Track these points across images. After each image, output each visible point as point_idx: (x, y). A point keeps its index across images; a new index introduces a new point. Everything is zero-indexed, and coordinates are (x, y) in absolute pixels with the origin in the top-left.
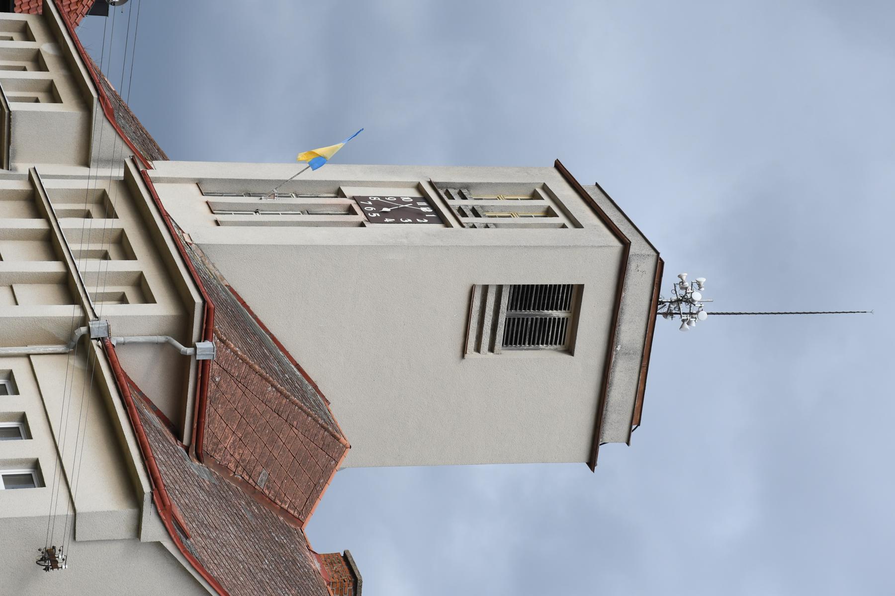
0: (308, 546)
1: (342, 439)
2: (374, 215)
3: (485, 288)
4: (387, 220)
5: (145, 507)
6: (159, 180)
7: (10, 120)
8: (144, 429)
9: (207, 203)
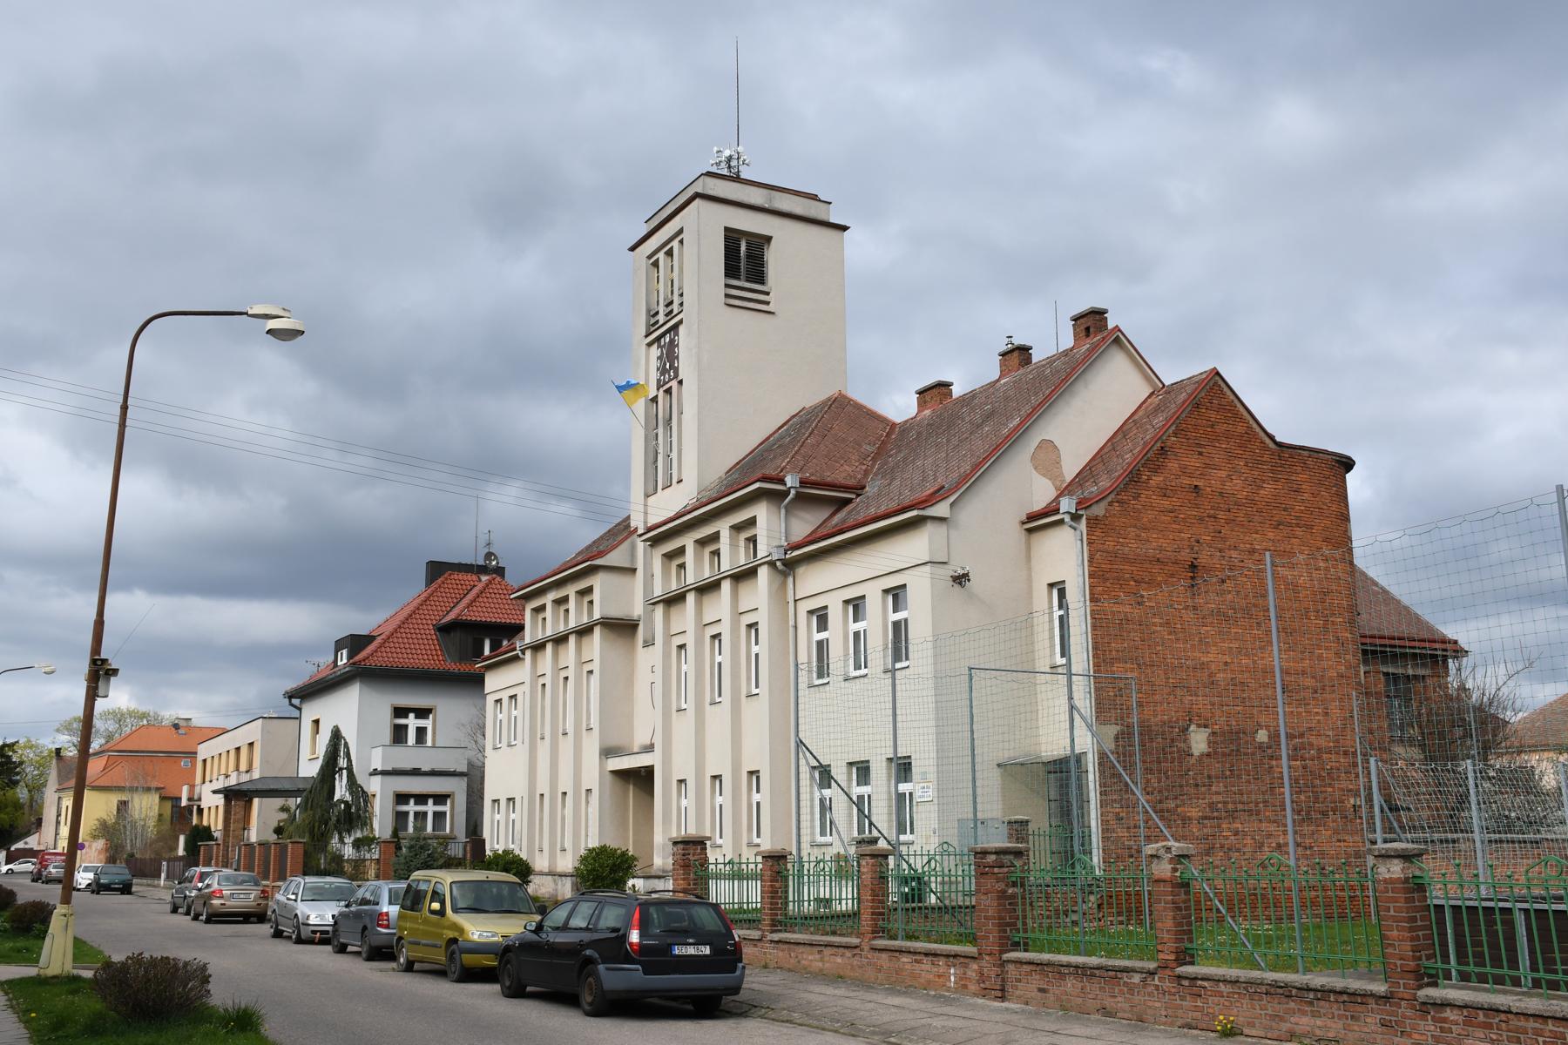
0: (912, 419)
1: (836, 396)
2: (672, 374)
3: (727, 296)
4: (676, 365)
5: (927, 514)
6: (645, 522)
7: (607, 618)
8: (851, 522)
9: (678, 482)
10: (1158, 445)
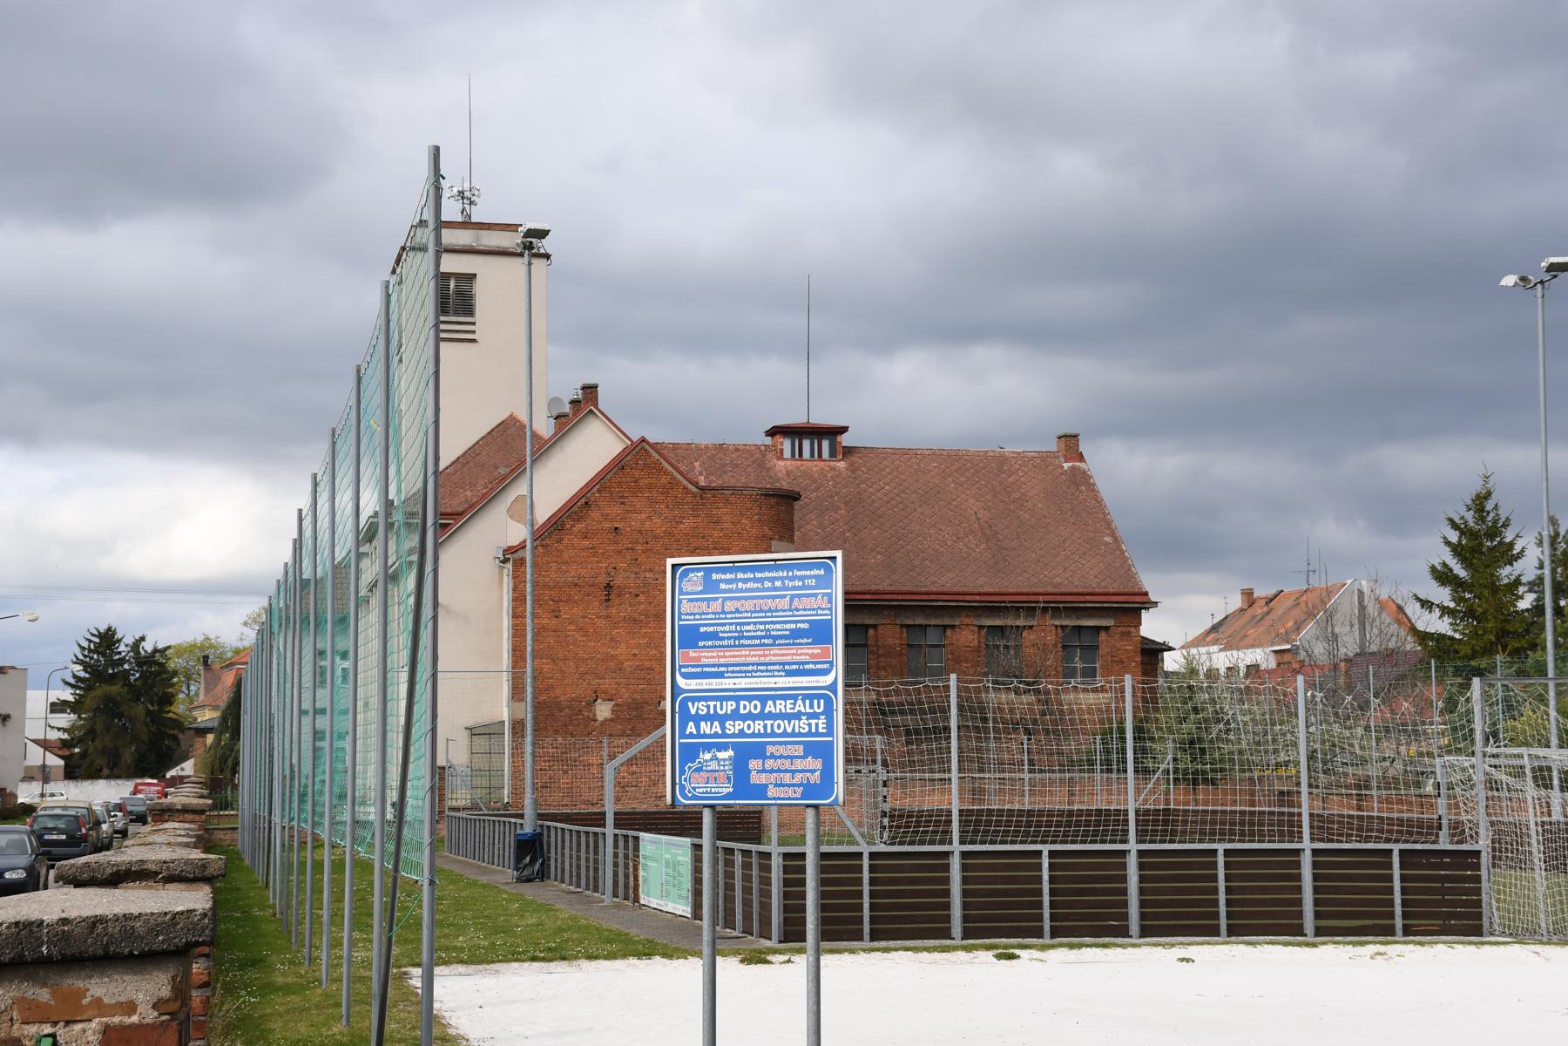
10: (583, 500)
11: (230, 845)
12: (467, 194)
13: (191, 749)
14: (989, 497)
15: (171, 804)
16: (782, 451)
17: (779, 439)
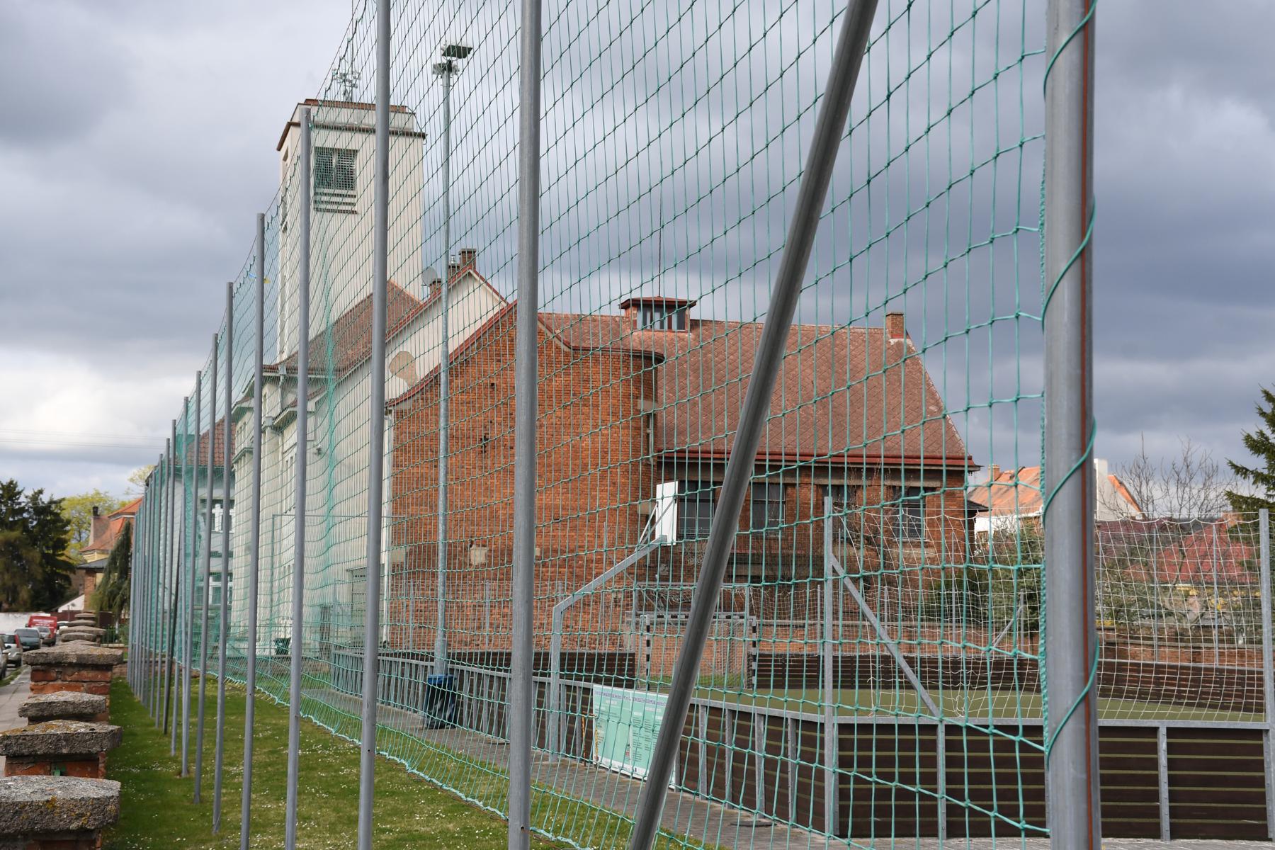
11: (119, 678)
12: (349, 77)
13: (81, 587)
14: (824, 368)
15: (61, 655)
16: (635, 322)
17: (632, 311)
